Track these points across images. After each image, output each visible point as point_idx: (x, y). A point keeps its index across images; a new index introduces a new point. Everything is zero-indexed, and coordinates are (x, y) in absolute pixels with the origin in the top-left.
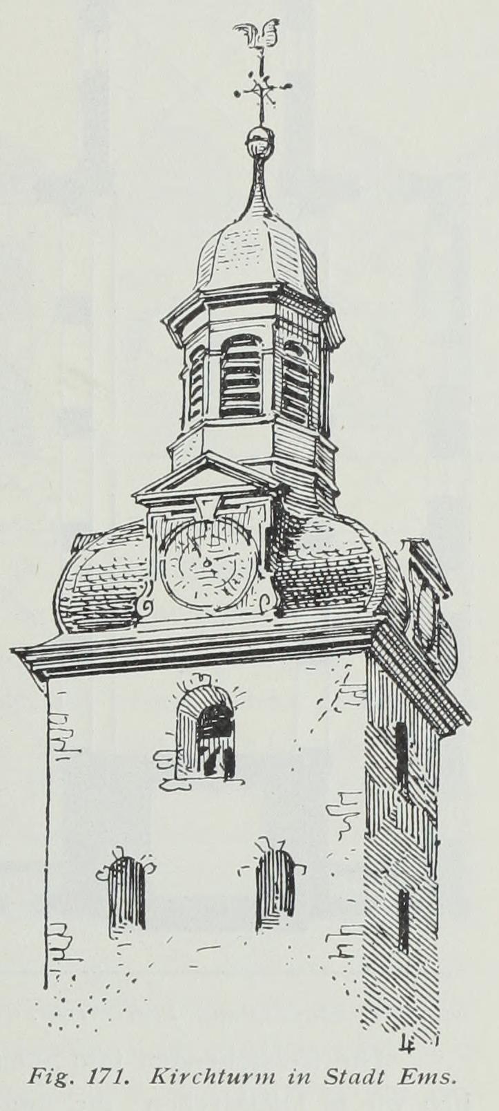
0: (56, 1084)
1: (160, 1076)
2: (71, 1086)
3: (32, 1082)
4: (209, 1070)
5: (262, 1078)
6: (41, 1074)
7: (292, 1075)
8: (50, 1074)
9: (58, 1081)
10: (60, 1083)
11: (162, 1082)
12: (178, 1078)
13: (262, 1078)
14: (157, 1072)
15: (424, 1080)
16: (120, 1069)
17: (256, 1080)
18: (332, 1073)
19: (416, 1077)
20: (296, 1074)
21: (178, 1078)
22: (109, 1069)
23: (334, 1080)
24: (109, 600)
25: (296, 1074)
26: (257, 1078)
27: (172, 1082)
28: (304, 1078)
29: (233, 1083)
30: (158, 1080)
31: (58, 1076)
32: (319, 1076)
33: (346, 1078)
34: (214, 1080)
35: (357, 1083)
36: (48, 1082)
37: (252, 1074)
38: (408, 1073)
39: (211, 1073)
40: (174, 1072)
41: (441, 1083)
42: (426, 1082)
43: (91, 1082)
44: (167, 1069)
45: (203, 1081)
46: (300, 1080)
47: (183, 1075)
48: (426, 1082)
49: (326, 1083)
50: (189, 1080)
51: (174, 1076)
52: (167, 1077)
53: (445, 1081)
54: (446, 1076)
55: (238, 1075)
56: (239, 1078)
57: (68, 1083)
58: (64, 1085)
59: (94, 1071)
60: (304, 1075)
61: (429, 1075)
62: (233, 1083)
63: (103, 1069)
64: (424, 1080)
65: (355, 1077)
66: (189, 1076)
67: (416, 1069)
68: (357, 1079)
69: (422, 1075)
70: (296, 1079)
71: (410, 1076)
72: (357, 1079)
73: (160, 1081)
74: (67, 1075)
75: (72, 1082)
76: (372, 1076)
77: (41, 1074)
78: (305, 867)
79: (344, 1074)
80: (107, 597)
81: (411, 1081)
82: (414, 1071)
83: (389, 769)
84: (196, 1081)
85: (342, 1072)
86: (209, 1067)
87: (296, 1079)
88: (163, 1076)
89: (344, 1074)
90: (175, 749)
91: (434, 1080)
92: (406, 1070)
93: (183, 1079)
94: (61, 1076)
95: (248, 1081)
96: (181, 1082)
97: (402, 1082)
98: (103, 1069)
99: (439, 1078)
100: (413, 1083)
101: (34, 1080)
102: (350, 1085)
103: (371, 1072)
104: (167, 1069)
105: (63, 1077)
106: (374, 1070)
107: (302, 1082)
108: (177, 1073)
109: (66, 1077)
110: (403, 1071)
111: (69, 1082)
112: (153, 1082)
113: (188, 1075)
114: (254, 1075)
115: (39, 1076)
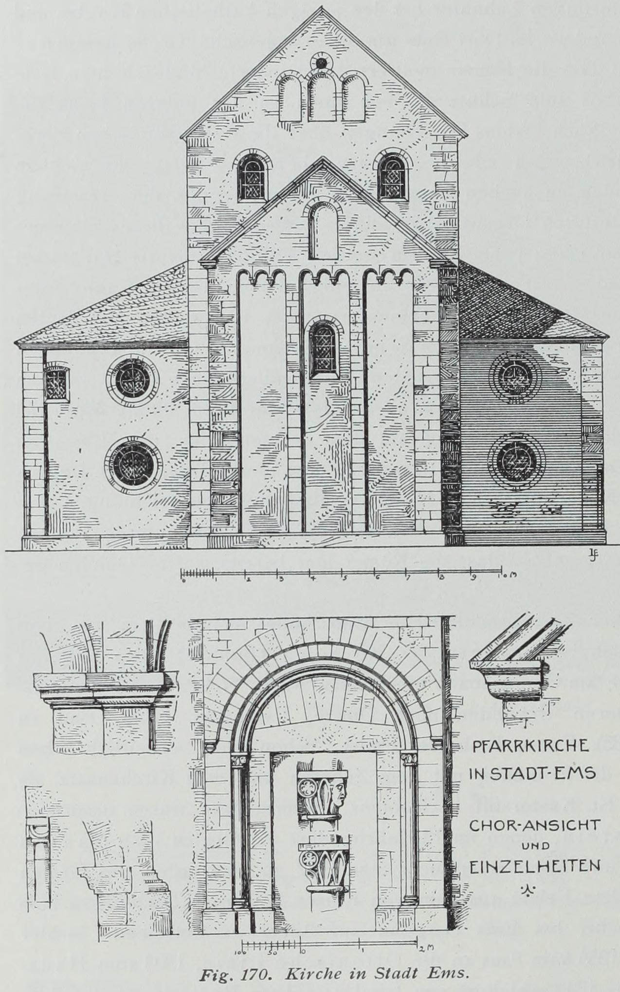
1: (293, 974)
3: (203, 980)
4: (328, 969)
7: (353, 973)
9: (221, 979)
10: (223, 980)
11: (295, 978)
12: (306, 975)
15: (446, 975)
16: (245, 969)
18: (380, 970)
19: (440, 973)
20: (356, 972)
21: (306, 975)
23: (381, 976)
24: (541, 511)
25: (356, 972)
27: (302, 978)
28: (362, 975)
30: (292, 976)
31: (221, 975)
32: (371, 973)
33: (390, 975)
34: (389, 975)
36: (214, 979)
38: (435, 970)
39: (329, 971)
40: (303, 971)
41: (458, 977)
42: (448, 977)
43: (244, 979)
44: (298, 969)
48: (448, 977)
49: (376, 978)
50: (313, 976)
51: (303, 973)
52: (298, 974)
53: (460, 976)
54: (461, 972)
56: (357, 975)
58: (226, 982)
59: (246, 971)
61: (449, 971)
64: (446, 975)
65: (397, 973)
67: (440, 967)
69: (444, 971)
70: (356, 975)
71: (436, 972)
73: (293, 977)
76: (409, 972)
79: (389, 971)
80: (542, 513)
81: (437, 976)
83: (558, 495)
84: (319, 977)
85: (387, 969)
87: (356, 975)
88: (295, 974)
89: (389, 971)
90: (207, 346)
91: (330, 976)
92: (433, 968)
94: (223, 975)
95: (310, 977)
96: (308, 978)
97: (430, 977)
99: (456, 974)
100: (437, 977)
104: (298, 969)
105: (225, 976)
106: (410, 968)
108: (305, 972)
110: (290, 970)
112: (288, 978)
115: (208, 975)
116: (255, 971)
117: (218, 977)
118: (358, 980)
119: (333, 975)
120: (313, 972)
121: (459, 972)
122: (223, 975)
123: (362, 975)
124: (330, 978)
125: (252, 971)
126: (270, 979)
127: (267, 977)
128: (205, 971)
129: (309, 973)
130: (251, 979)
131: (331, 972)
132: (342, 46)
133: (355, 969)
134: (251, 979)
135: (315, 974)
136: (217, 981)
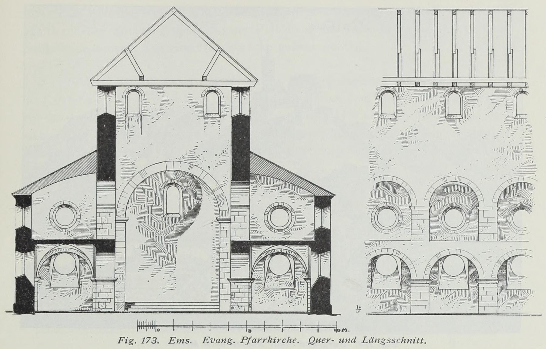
0: (227, 343)
2: (135, 344)
3: (119, 343)
4: (403, 337)
5: (420, 341)
6: (123, 339)
8: (127, 340)
9: (228, 342)
13: (420, 341)
14: (121, 339)
16: (144, 337)
17: (263, 341)
19: (176, 340)
22: (150, 338)
26: (263, 340)
29: (318, 342)
31: (130, 340)
35: (255, 342)
36: (126, 343)
37: (261, 339)
38: (206, 339)
39: (404, 339)
41: (186, 343)
42: (180, 343)
43: (143, 343)
45: (286, 342)
46: (222, 341)
47: (278, 339)
48: (180, 343)
50: (281, 341)
54: (188, 340)
55: (343, 339)
57: (232, 343)
60: (377, 339)
62: (318, 342)
63: (147, 338)
66: (267, 340)
67: (176, 338)
68: (372, 341)
69: (178, 340)
72: (372, 341)
74: (133, 340)
75: (135, 343)
77: (123, 339)
78: (492, 202)
81: (207, 342)
82: (175, 338)
84: (398, 342)
85: (418, 338)
86: (356, 336)
92: (172, 338)
93: (278, 341)
94: (230, 340)
98: (147, 338)
99: (185, 341)
100: (174, 343)
101: (120, 342)
102: (252, 344)
103: (355, 338)
107: (181, 343)
108: (416, 339)
109: (232, 340)
111: (134, 343)
113: (281, 339)
114: (262, 339)
115: (122, 340)
116: (149, 339)
117: (128, 341)
118: (346, 344)
119: (292, 341)
120: (281, 339)
121: (187, 341)
122: (230, 340)
123: (318, 341)
124: (349, 342)
125: (148, 339)
126: (158, 343)
127: (157, 342)
128: (121, 338)
129: (278, 339)
130: (147, 343)
131: (291, 339)
132: (456, 127)
133: (276, 338)
134: (147, 343)
135: (282, 340)
136: (380, 343)
